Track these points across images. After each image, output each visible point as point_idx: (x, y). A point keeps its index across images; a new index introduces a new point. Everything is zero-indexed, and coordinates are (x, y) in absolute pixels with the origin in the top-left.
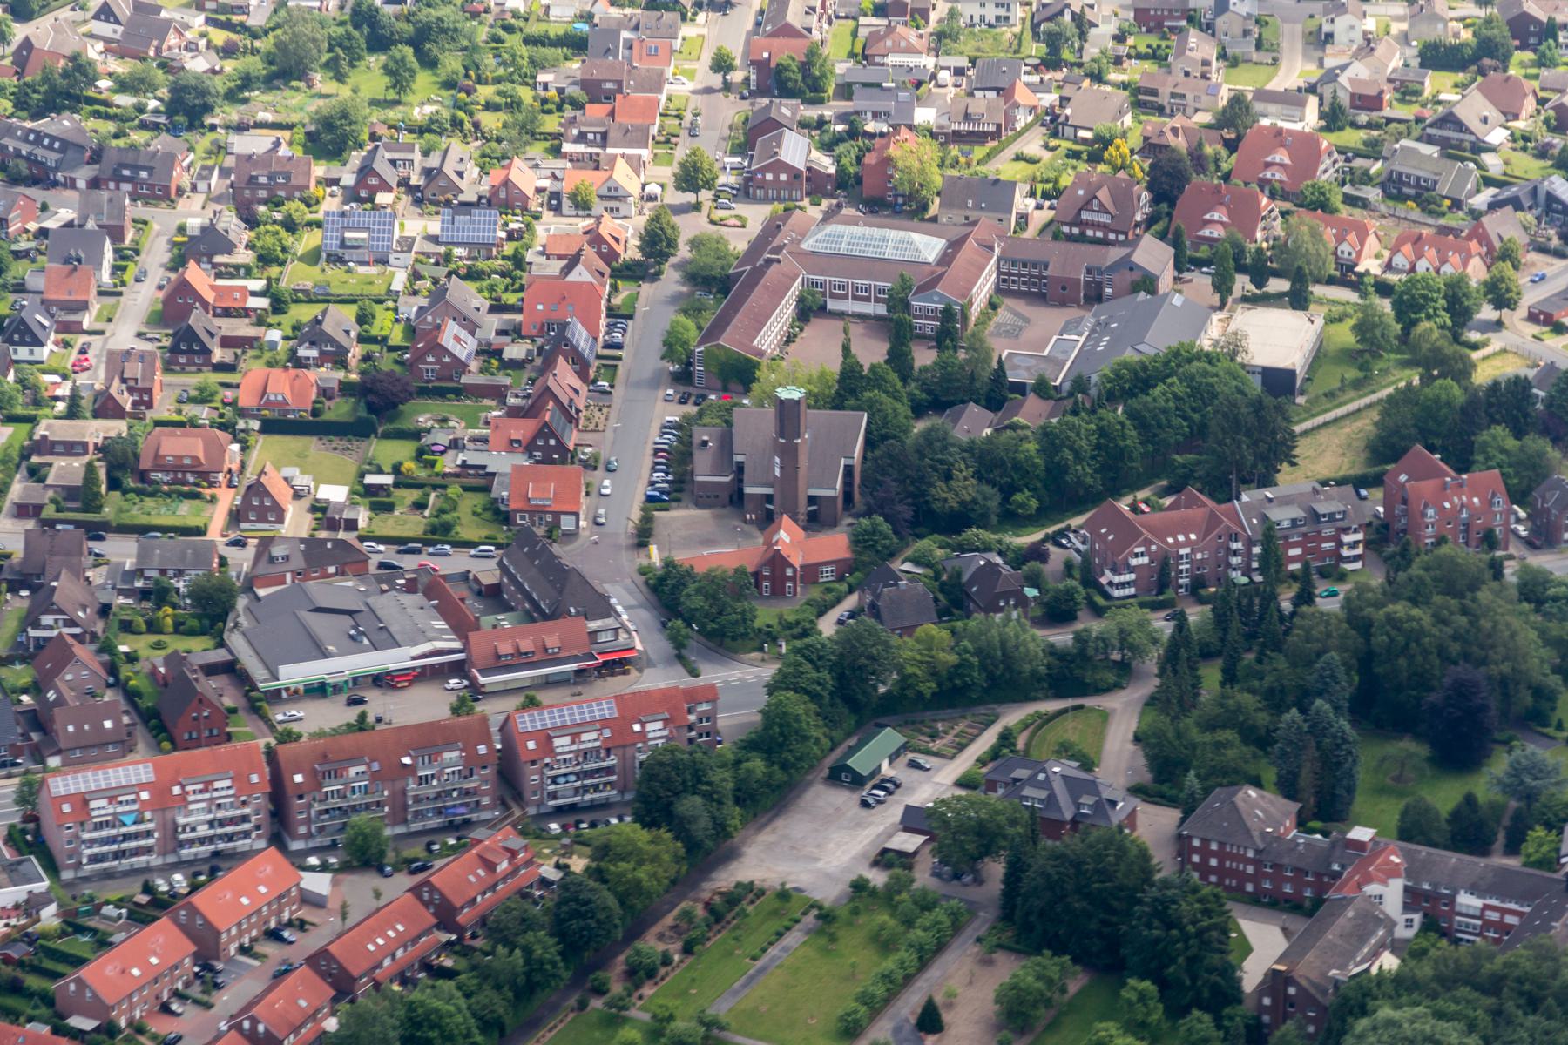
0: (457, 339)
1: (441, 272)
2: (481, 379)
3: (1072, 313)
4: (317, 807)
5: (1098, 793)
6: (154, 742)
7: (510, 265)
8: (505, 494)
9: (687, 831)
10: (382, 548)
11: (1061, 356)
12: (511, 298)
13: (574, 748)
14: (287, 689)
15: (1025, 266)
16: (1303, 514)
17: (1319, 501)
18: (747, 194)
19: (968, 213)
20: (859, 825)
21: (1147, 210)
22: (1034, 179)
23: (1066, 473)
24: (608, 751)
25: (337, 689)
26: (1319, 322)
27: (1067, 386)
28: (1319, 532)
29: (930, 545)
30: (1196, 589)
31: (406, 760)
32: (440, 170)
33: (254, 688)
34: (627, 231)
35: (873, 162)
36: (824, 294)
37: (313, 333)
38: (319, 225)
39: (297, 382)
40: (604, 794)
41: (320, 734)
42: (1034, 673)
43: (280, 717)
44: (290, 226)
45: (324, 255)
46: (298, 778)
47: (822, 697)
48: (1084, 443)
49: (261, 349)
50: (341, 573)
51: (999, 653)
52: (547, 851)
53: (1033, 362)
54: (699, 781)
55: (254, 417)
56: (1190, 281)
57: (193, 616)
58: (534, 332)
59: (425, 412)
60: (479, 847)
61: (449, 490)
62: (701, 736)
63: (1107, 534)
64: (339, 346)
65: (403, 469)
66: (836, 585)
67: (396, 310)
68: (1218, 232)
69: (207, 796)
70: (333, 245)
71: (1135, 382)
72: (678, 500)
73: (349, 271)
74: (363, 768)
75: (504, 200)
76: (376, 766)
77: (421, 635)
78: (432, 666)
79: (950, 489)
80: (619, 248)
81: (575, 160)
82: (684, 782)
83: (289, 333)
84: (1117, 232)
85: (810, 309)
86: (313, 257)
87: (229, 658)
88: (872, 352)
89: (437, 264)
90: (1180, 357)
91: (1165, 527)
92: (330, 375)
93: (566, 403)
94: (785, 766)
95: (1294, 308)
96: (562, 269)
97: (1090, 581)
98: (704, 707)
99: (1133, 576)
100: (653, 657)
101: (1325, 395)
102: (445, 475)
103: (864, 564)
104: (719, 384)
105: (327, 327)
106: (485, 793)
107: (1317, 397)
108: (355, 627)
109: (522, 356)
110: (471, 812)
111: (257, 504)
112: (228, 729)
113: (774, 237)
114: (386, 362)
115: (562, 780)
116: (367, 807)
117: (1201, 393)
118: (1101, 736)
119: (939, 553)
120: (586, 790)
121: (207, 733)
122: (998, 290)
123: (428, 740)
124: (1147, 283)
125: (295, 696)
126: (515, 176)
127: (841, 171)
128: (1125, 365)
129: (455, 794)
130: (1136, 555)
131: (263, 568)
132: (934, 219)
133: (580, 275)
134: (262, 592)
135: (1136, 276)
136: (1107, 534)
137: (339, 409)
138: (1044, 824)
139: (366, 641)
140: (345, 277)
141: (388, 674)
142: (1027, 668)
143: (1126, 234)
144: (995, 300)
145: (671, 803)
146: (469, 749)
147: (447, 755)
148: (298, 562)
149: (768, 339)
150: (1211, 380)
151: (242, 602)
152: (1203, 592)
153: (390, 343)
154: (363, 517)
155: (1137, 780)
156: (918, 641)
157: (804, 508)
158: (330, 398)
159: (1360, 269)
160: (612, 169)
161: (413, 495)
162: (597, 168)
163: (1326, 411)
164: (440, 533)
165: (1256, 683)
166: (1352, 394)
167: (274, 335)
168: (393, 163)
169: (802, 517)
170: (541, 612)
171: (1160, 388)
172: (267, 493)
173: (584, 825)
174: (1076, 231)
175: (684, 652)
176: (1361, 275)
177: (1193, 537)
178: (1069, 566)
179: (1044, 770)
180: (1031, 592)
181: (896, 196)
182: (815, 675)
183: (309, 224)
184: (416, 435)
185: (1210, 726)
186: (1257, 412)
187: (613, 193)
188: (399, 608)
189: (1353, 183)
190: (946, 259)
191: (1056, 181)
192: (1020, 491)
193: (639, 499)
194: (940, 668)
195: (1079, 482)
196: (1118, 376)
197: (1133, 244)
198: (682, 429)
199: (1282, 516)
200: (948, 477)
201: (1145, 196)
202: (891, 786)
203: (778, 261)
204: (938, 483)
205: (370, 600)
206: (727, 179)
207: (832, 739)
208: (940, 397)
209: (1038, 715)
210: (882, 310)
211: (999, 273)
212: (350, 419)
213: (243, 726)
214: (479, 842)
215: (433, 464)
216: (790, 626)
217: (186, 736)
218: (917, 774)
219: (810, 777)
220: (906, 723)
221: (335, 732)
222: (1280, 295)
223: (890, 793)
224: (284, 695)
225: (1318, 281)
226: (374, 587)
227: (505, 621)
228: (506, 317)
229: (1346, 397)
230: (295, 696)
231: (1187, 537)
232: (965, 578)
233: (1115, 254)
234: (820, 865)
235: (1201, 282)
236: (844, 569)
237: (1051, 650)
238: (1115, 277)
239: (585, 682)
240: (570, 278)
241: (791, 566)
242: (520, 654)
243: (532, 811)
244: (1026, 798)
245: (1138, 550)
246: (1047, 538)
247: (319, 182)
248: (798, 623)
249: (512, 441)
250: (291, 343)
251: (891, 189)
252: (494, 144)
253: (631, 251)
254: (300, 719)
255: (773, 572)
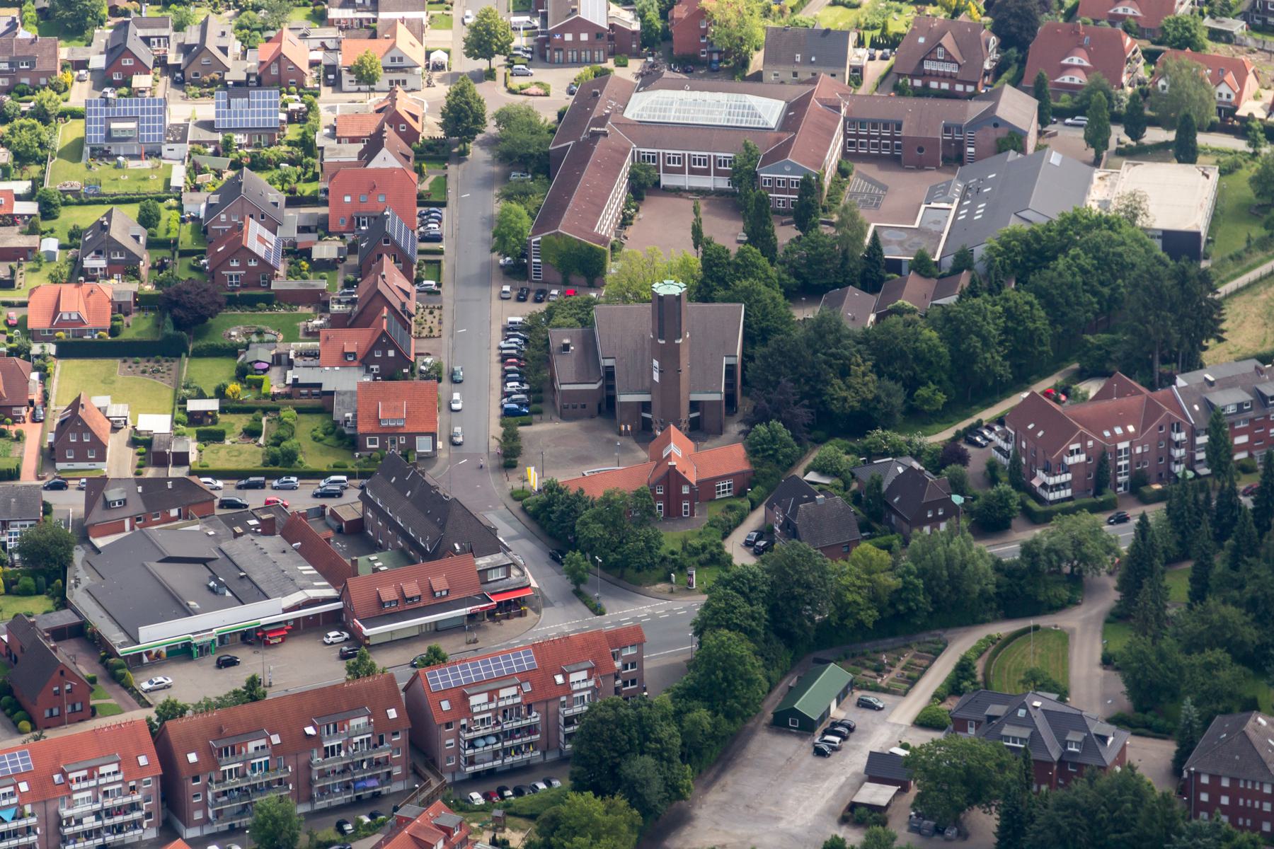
0: (261, 239)
1: (223, 162)
2: (294, 284)
3: (934, 177)
4: (216, 789)
5: (1084, 728)
6: (9, 721)
7: (298, 152)
8: (349, 415)
9: (640, 796)
10: (220, 483)
11: (934, 228)
12: (307, 189)
13: (493, 706)
14: (148, 653)
15: (875, 126)
16: (1248, 398)
17: (1264, 382)
18: (543, 57)
19: (796, 69)
20: (817, 776)
21: (995, 56)
22: (858, 26)
23: (974, 362)
24: (529, 708)
25: (204, 649)
26: (1214, 175)
27: (949, 261)
28: (1267, 417)
29: (831, 450)
30: (1137, 487)
31: (310, 730)
32: (202, 47)
33: (111, 653)
34: (425, 106)
35: (684, 15)
36: (657, 168)
37: (99, 240)
38: (76, 115)
39: (92, 298)
40: (526, 756)
41: (208, 706)
42: (983, 592)
43: (146, 686)
44: (42, 115)
45: (87, 149)
46: (192, 758)
47: (758, 633)
48: (991, 328)
49: (38, 261)
50: (183, 515)
51: (945, 573)
52: (475, 825)
53: (904, 235)
54: (647, 738)
55: (47, 340)
56: (1055, 134)
57: (24, 573)
58: (343, 227)
59: (235, 325)
60: (411, 826)
61: (282, 414)
62: (626, 684)
63: (1035, 430)
64: (130, 254)
65: (228, 392)
66: (737, 502)
67: (180, 208)
68: (1079, 79)
69: (93, 783)
70: (97, 137)
71: (1029, 256)
72: (539, 412)
73: (118, 166)
74: (263, 742)
75: (276, 76)
76: (276, 739)
77: (291, 584)
78: (306, 618)
79: (849, 387)
80: (417, 126)
81: (345, 27)
82: (630, 740)
83: (66, 241)
84: (965, 83)
85: (644, 186)
86: (74, 151)
87: (77, 620)
88: (728, 234)
89: (216, 154)
90: (1077, 226)
91: (1106, 418)
92: (117, 288)
93: (399, 308)
94: (730, 716)
95: (1180, 161)
96: (361, 154)
97: (1020, 480)
98: (630, 652)
99: (1069, 477)
100: (547, 594)
101: (1231, 258)
102: (274, 397)
103: (764, 476)
104: (559, 278)
105: (116, 232)
106: (396, 763)
107: (1223, 260)
108: (214, 577)
109: (334, 255)
110: (382, 785)
111: (75, 438)
112: (92, 703)
113: (593, 107)
114: (181, 271)
115: (481, 743)
116: (269, 785)
117: (1109, 264)
118: (1063, 659)
119: (847, 459)
120: (507, 752)
121: (69, 709)
122: (845, 154)
123: (329, 706)
124: (1015, 139)
125: (158, 659)
126: (287, 50)
127: (647, 25)
128: (1014, 235)
129: (365, 766)
130: (1072, 453)
131: (98, 515)
132: (758, 77)
133: (386, 160)
134: (100, 542)
135: (1001, 133)
136: (1035, 430)
137: (137, 327)
138: (1036, 769)
139: (228, 594)
140: (115, 173)
141: (258, 629)
142: (977, 588)
143: (975, 84)
144: (844, 166)
145: (618, 765)
146: (378, 715)
147: (353, 722)
148: (137, 507)
149: (606, 225)
150: (1120, 249)
151: (79, 555)
152: (1144, 490)
153: (181, 247)
154: (192, 447)
155: (1114, 711)
156: (854, 563)
157: (686, 415)
158: (126, 314)
159: (1242, 112)
160: (394, 35)
161: (241, 422)
162: (374, 36)
163: (1235, 276)
164: (281, 464)
165: (1236, 593)
166: (1260, 255)
167: (50, 244)
168: (146, 40)
169: (684, 426)
170: (422, 551)
171: (1061, 262)
172: (86, 428)
173: (509, 793)
174: (918, 83)
175: (582, 587)
176: (1242, 120)
177: (1131, 429)
178: (992, 467)
179: (1024, 706)
180: (957, 499)
181: (711, 53)
182: (748, 609)
183: (63, 115)
184: (232, 352)
185: (1193, 645)
186: (1182, 283)
187: (397, 64)
188: (260, 553)
189: (1212, 15)
190: (791, 121)
191: (885, 27)
192: (925, 384)
193: (496, 412)
194: (881, 591)
195: (989, 371)
196: (1005, 245)
197: (994, 96)
198: (530, 331)
199: (1227, 400)
200: (844, 373)
201: (994, 40)
202: (845, 731)
203: (605, 134)
204: (835, 381)
205: (224, 546)
206: (520, 41)
207: (769, 679)
208: (811, 281)
209: (991, 640)
210: (723, 183)
211: (846, 136)
212: (147, 337)
213: (105, 696)
214: (409, 820)
215: (259, 385)
216: (695, 552)
217: (47, 714)
218: (869, 715)
219: (751, 725)
220: (846, 657)
221: (222, 704)
222: (1164, 145)
223: (844, 738)
224: (145, 659)
225: (1201, 130)
226: (224, 530)
227: (379, 561)
228: (305, 211)
229: (1255, 260)
230: (158, 659)
231: (1125, 430)
232: (885, 487)
233: (975, 109)
234: (782, 825)
235: (1071, 135)
236: (742, 485)
237: (998, 566)
238: (977, 134)
239: (478, 628)
240: (372, 165)
241: (687, 483)
242: (404, 598)
243: (448, 778)
244: (1007, 738)
245: (1074, 447)
246: (959, 435)
247: (64, 68)
248: (704, 547)
249: (346, 355)
250: (71, 252)
251: (705, 45)
252: (251, 14)
253: (431, 127)
254: (169, 687)
255: (667, 491)
